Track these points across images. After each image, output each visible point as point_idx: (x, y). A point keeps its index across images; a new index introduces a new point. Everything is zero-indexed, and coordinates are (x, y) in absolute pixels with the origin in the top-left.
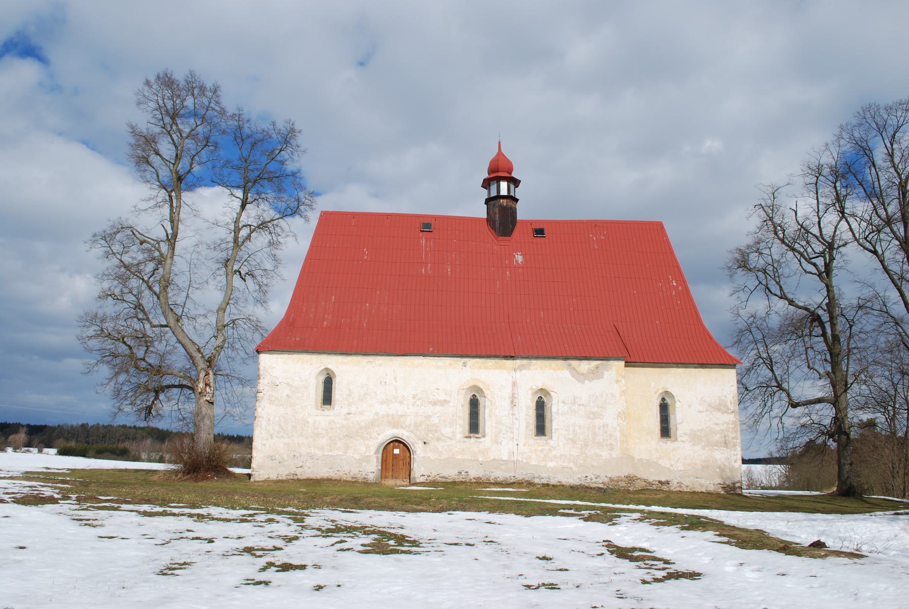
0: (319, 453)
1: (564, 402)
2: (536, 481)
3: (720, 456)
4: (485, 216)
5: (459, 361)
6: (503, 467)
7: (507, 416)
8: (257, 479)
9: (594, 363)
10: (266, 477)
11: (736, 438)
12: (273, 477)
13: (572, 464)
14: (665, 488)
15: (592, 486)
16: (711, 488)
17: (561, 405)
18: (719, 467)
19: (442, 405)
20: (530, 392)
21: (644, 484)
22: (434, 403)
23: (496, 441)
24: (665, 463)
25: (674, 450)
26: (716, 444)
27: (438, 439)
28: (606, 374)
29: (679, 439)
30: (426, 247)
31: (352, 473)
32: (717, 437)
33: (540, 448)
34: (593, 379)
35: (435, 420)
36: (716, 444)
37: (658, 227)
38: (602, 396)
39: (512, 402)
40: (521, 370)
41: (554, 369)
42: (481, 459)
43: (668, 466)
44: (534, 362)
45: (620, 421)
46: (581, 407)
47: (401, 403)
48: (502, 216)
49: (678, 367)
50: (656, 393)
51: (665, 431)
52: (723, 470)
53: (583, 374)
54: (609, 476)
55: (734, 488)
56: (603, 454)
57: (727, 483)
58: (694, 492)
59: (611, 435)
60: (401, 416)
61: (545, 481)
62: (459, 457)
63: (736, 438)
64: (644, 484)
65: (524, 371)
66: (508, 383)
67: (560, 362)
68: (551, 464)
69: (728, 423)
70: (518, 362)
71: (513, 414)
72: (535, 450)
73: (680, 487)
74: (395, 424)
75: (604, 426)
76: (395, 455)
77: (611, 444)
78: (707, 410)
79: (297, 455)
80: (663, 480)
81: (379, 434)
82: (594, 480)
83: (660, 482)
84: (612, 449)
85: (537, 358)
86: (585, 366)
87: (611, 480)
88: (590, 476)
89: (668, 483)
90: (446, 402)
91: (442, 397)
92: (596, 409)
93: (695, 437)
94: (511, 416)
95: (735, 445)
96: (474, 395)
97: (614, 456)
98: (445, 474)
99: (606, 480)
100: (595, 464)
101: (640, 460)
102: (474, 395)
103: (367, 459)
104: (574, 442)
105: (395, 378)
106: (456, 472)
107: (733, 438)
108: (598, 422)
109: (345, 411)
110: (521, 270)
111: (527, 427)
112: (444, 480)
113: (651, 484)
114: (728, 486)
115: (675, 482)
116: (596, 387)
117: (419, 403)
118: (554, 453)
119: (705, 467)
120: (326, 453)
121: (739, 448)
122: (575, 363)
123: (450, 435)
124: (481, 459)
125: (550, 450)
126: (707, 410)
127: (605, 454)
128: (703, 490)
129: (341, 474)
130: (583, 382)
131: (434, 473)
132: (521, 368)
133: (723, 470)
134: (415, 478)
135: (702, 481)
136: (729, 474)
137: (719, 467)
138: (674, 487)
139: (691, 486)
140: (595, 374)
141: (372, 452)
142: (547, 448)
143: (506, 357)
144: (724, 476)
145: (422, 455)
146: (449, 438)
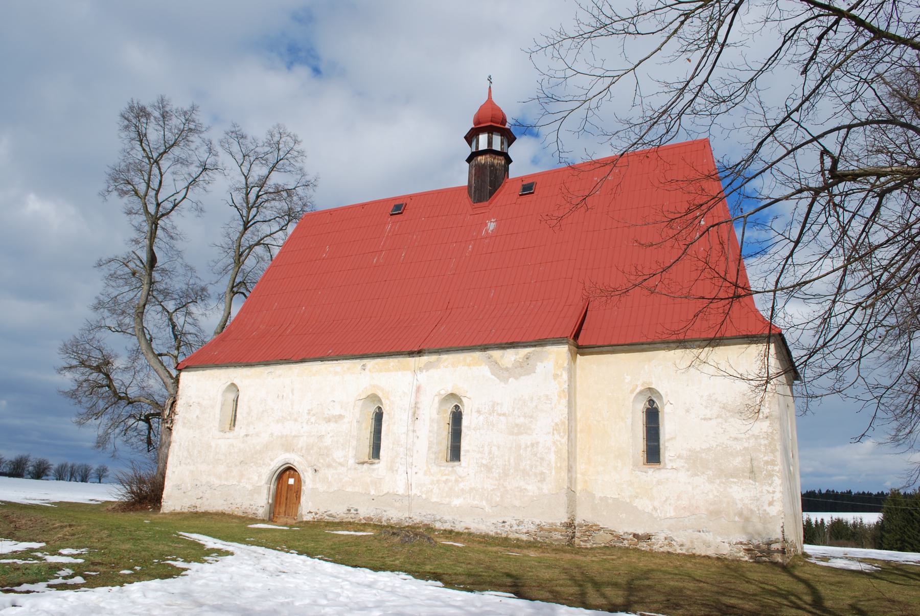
0: (217, 482)
1: (479, 412)
2: (438, 525)
3: (741, 494)
4: (466, 184)
5: (357, 364)
6: (397, 504)
7: (414, 435)
8: (166, 511)
9: (523, 352)
10: (172, 508)
11: (772, 462)
12: (178, 509)
13: (484, 503)
14: (643, 546)
15: (511, 536)
16: (725, 550)
17: (475, 415)
18: (740, 514)
19: (336, 422)
20: (437, 399)
21: (610, 537)
22: (329, 420)
23: (392, 469)
24: (643, 504)
25: (659, 483)
26: (734, 474)
27: (329, 466)
28: (540, 367)
29: (669, 466)
30: (390, 231)
31: (244, 507)
32: (737, 462)
33: (444, 478)
34: (521, 375)
35: (328, 441)
36: (734, 474)
37: (465, 138)
38: (532, 399)
39: (414, 413)
40: (427, 370)
41: (469, 365)
42: (373, 492)
43: (649, 509)
44: (444, 357)
45: (557, 437)
46: (502, 418)
47: (296, 420)
48: (488, 176)
49: (669, 349)
50: (632, 391)
51: (653, 454)
52: (747, 520)
53: (507, 369)
54: (538, 522)
55: (769, 552)
56: (529, 487)
57: (755, 542)
58: (693, 556)
59: (542, 459)
60: (295, 436)
61: (448, 526)
62: (349, 489)
63: (772, 462)
64: (610, 537)
65: (432, 371)
66: (413, 386)
67: (477, 355)
68: (456, 502)
69: (757, 437)
70: (425, 359)
71: (414, 431)
72: (438, 481)
73: (670, 545)
74: (288, 448)
75: (532, 445)
76: (289, 485)
77: (542, 473)
78: (718, 417)
79: (199, 484)
80: (640, 532)
81: (272, 460)
82: (515, 527)
83: (635, 535)
84: (542, 481)
85: (448, 351)
86: (510, 356)
87: (540, 528)
88: (510, 521)
89: (648, 537)
90: (341, 417)
91: (337, 411)
92: (522, 420)
93: (696, 462)
94: (411, 434)
95: (770, 475)
96: (456, 406)
97: (545, 491)
98: (332, 512)
99: (533, 528)
100: (517, 503)
101: (604, 499)
102: (456, 406)
103: (256, 490)
104: (489, 468)
105: (293, 390)
106: (345, 510)
107: (767, 463)
108: (525, 440)
109: (243, 432)
110: (487, 241)
111: (430, 448)
112: (331, 519)
113: (619, 538)
114: (758, 547)
115: (662, 536)
116: (525, 386)
117: (313, 419)
118: (461, 485)
119: (715, 513)
120: (224, 482)
121: (777, 481)
122: (496, 354)
123: (342, 460)
124: (373, 492)
125: (456, 481)
126: (718, 417)
127: (532, 488)
128: (711, 552)
129: (234, 507)
130: (505, 380)
131: (322, 510)
132: (428, 366)
133: (747, 520)
134: (302, 516)
135: (709, 537)
136: (759, 526)
137: (740, 514)
138: (659, 545)
139: (688, 544)
140: (525, 367)
141: (264, 482)
142: (453, 478)
143: (411, 354)
144: (750, 529)
145: (310, 486)
146: (340, 464)
